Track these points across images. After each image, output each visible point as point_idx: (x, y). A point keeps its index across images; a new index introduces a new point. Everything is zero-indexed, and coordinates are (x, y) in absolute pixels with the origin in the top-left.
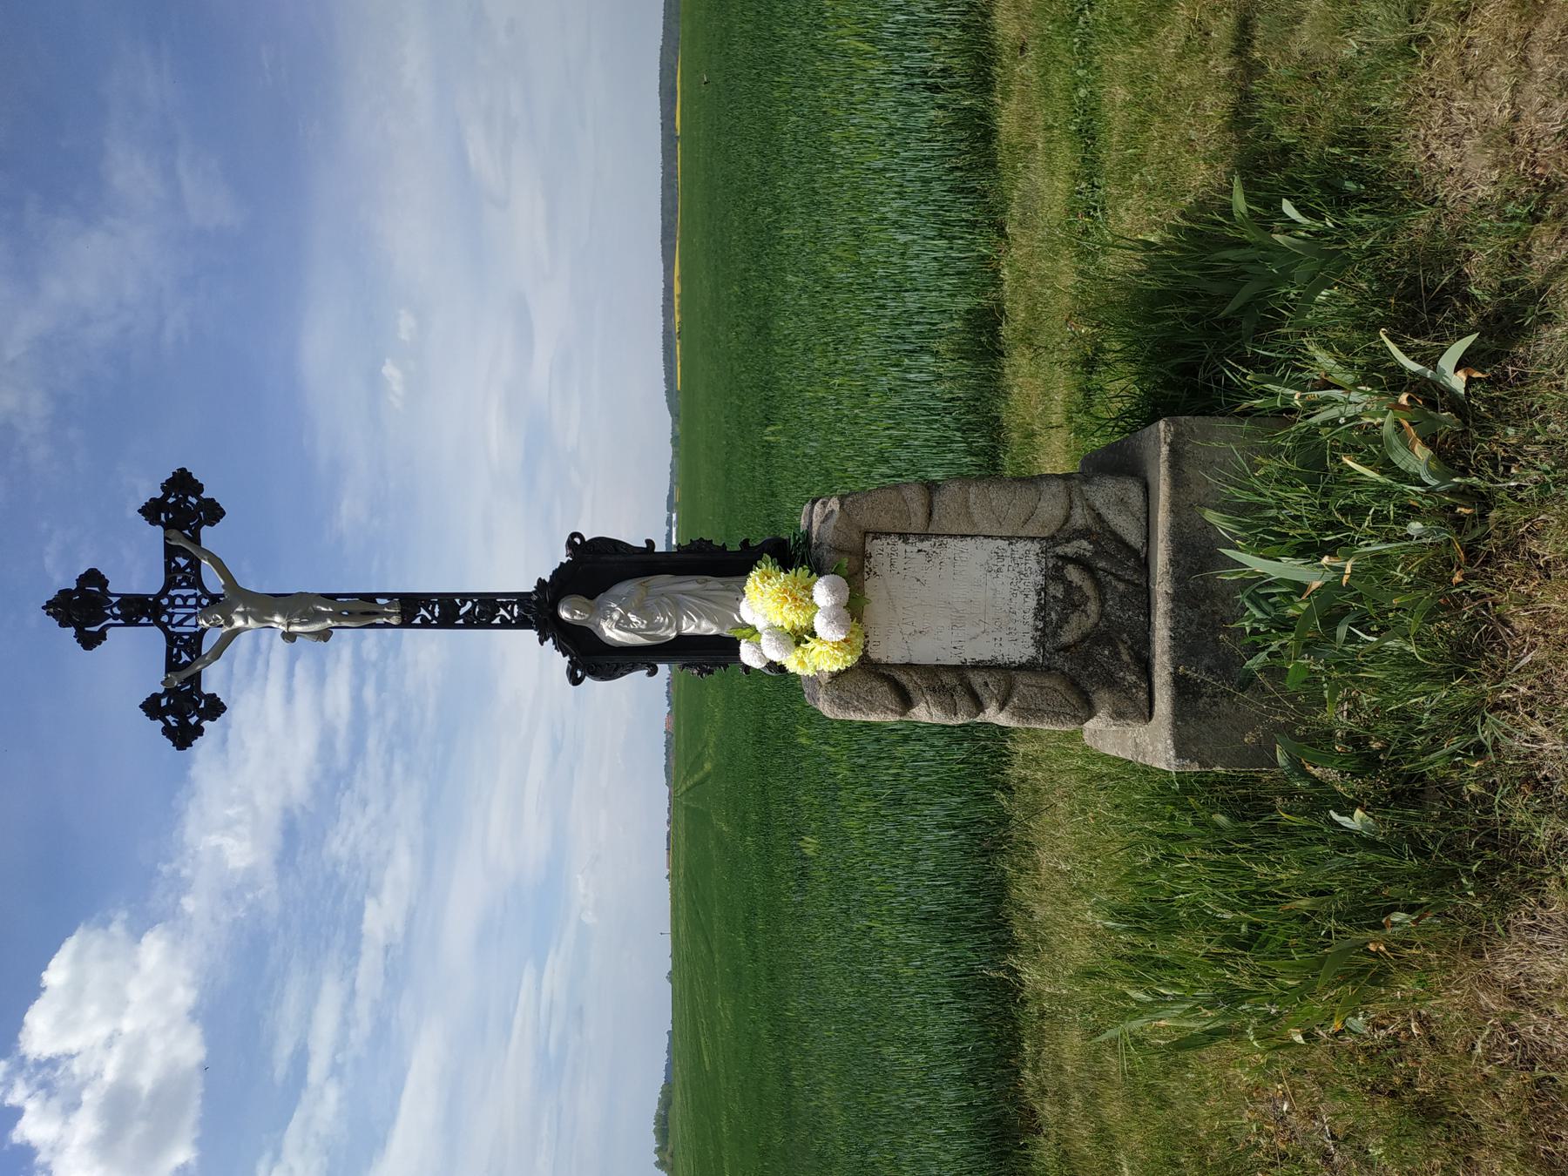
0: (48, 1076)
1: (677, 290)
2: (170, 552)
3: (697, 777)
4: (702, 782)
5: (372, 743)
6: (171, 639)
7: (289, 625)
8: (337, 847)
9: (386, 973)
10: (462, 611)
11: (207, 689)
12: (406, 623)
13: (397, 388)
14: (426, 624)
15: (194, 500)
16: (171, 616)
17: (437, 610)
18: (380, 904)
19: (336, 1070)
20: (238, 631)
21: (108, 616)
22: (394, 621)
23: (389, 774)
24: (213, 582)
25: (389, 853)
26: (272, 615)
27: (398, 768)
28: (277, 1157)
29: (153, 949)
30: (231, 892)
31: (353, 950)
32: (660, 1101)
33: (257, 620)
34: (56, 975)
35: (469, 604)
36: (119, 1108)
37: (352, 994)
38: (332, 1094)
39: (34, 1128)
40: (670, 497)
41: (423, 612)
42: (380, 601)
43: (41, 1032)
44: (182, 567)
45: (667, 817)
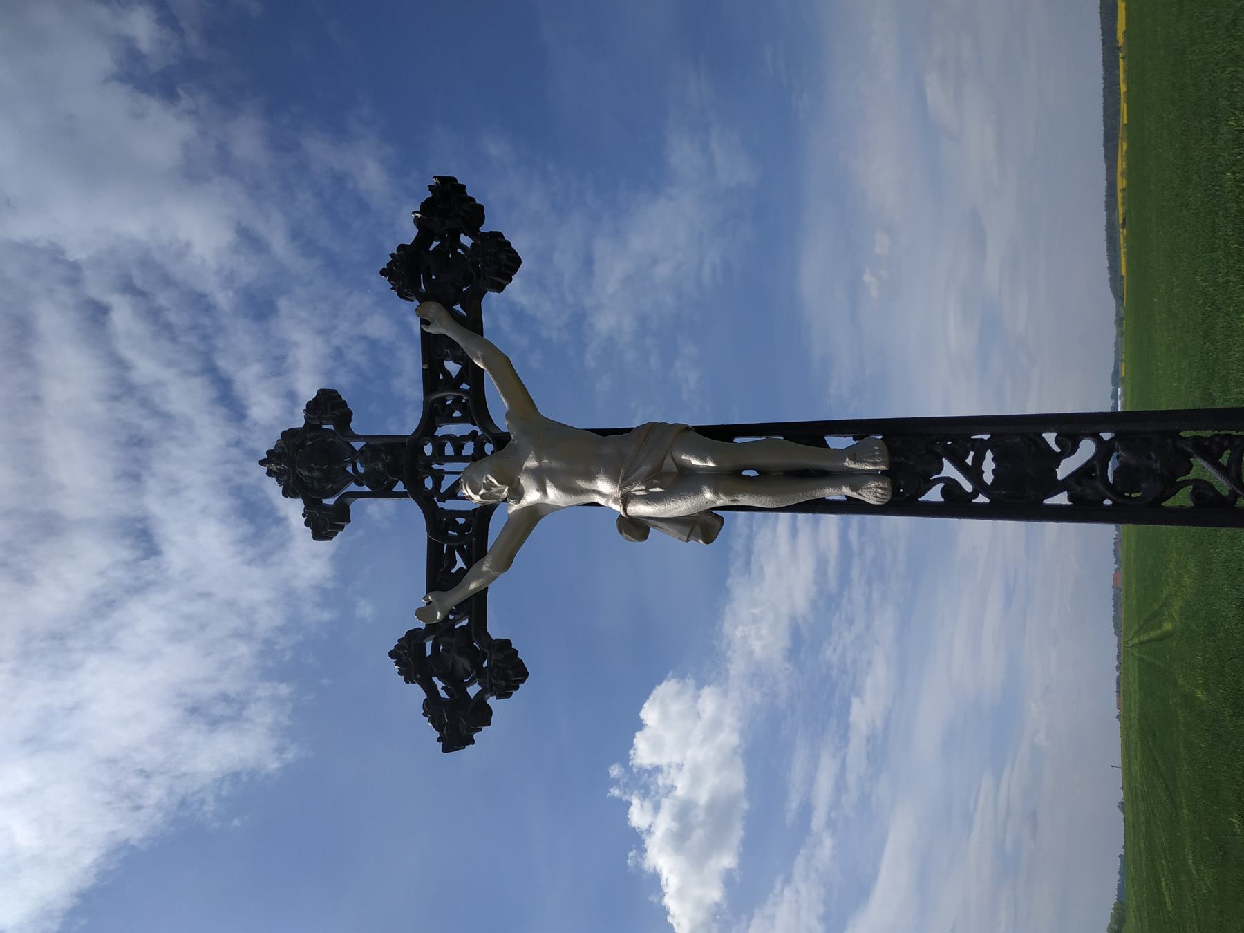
0: (645, 782)
1: (1121, 183)
2: (433, 349)
3: (1152, 634)
4: (1159, 639)
5: (855, 572)
6: (438, 523)
7: (626, 500)
8: (830, 654)
9: (868, 757)
10: (1065, 469)
11: (495, 629)
12: (904, 502)
13: (874, 292)
14: (957, 505)
15: (466, 240)
16: (438, 477)
17: (988, 465)
18: (863, 703)
19: (830, 824)
20: (534, 514)
21: (349, 479)
22: (871, 494)
23: (869, 599)
24: (498, 405)
25: (869, 663)
26: (591, 477)
27: (876, 596)
28: (788, 880)
29: (709, 702)
30: (757, 676)
31: (845, 739)
32: (1112, 917)
33: (566, 489)
34: (650, 714)
35: (1087, 449)
36: (684, 812)
37: (843, 768)
38: (828, 842)
39: (638, 816)
40: (1116, 373)
41: (949, 470)
42: (836, 442)
43: (643, 752)
44: (453, 385)
45: (1116, 663)
